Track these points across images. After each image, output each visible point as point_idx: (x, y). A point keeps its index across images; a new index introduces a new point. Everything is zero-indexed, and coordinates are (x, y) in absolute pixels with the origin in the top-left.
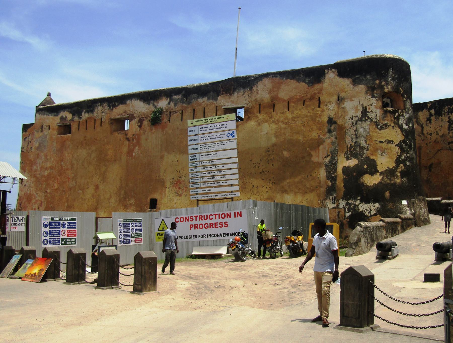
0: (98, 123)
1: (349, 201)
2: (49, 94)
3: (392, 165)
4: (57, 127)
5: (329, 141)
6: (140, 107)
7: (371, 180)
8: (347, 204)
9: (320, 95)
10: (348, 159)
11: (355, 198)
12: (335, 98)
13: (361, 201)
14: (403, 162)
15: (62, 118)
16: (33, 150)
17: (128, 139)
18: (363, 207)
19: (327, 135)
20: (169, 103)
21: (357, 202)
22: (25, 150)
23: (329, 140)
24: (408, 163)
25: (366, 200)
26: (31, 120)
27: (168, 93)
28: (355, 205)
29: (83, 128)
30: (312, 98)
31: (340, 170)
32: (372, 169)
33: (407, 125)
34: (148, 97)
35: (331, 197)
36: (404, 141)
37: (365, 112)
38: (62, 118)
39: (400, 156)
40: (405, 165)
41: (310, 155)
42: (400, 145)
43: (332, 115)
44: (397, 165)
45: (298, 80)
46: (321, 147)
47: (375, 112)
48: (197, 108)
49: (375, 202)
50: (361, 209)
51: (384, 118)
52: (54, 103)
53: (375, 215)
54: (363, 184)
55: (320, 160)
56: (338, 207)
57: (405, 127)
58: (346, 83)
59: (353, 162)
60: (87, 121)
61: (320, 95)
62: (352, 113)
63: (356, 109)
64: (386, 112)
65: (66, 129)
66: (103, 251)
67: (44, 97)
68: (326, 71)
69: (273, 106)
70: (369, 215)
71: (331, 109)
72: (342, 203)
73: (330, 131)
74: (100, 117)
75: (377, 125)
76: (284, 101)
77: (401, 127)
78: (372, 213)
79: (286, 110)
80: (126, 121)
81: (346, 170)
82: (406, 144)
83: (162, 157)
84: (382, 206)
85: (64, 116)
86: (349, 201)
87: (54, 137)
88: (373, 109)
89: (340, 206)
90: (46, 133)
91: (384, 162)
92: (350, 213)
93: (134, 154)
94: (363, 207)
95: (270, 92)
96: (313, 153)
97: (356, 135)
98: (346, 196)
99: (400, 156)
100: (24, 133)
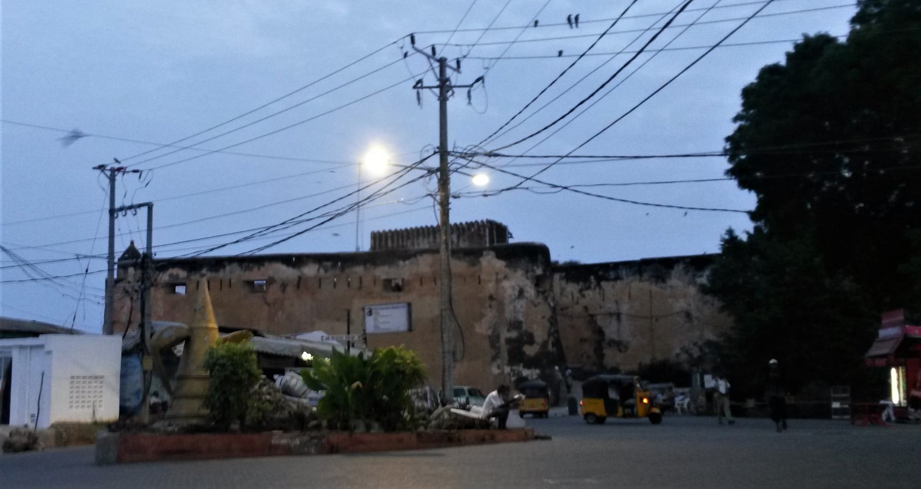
2: (132, 243)
6: (639, 285)
7: (530, 351)
8: (512, 370)
10: (509, 330)
12: (494, 277)
13: (524, 367)
15: (171, 276)
17: (268, 304)
18: (526, 372)
19: (489, 310)
20: (318, 270)
21: (521, 369)
23: (490, 315)
31: (503, 341)
32: (531, 340)
37: (521, 293)
38: (171, 276)
39: (550, 330)
45: (460, 259)
46: (483, 320)
47: (530, 291)
49: (536, 368)
51: (537, 296)
56: (503, 373)
57: (552, 304)
58: (500, 264)
59: (514, 334)
62: (509, 292)
63: (513, 288)
68: (485, 253)
71: (490, 287)
72: (507, 369)
73: (491, 306)
75: (532, 303)
77: (549, 305)
80: (893, 371)
81: (509, 341)
94: (526, 372)
98: (511, 362)
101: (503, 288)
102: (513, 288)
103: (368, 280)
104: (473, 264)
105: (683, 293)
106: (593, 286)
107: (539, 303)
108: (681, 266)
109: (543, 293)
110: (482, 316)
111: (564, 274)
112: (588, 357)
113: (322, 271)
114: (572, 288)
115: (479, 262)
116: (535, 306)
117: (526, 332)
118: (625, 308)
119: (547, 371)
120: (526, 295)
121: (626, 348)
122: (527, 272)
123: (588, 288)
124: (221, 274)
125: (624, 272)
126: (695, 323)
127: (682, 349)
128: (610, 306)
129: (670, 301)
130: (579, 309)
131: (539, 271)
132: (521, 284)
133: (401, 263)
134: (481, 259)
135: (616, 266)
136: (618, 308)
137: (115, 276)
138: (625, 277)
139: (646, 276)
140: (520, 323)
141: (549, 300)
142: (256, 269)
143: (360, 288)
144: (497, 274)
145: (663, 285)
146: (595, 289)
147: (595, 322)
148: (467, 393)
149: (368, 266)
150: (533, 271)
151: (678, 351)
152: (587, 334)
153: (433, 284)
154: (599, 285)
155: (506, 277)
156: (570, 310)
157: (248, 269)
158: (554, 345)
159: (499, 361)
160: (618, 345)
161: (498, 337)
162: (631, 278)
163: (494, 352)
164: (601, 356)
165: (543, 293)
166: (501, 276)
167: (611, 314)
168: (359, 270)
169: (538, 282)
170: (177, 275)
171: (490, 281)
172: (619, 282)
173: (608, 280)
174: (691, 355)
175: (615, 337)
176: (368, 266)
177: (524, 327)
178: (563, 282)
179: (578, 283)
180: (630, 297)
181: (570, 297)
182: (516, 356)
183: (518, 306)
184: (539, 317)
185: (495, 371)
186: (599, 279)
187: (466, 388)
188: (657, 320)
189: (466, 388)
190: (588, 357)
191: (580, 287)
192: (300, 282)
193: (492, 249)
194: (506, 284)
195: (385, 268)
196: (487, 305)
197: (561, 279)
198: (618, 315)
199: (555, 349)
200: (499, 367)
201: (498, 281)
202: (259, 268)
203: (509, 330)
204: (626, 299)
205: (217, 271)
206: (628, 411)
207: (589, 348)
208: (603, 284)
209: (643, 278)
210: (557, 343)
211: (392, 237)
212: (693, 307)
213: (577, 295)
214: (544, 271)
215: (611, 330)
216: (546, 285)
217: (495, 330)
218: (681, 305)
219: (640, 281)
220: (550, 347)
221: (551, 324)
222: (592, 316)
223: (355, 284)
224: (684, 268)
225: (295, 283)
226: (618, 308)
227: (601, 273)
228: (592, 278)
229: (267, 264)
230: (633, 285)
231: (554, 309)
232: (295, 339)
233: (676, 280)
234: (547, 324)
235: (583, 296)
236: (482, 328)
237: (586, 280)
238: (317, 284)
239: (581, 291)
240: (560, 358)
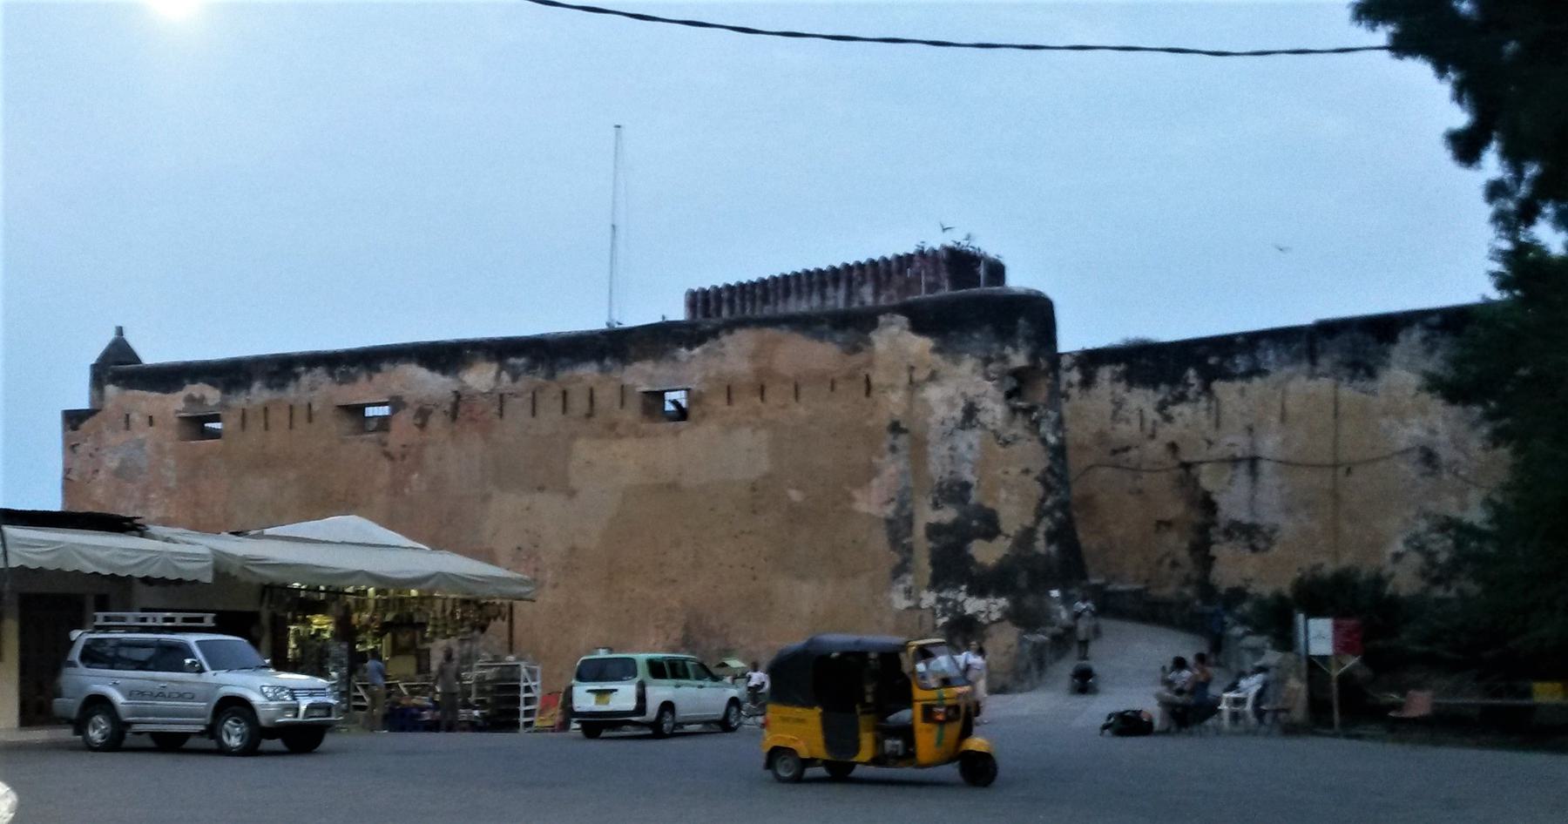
0: (300, 414)
1: (943, 595)
2: (120, 331)
3: (1029, 521)
4: (175, 421)
5: (892, 469)
6: (1304, 386)
7: (986, 553)
8: (939, 600)
9: (868, 371)
10: (936, 506)
11: (956, 587)
13: (970, 593)
14: (1049, 513)
15: (190, 399)
16: (102, 476)
17: (388, 455)
18: (973, 605)
19: (889, 457)
21: (961, 597)
22: (74, 477)
23: (892, 468)
24: (1058, 515)
25: (979, 590)
26: (81, 400)
27: (500, 350)
28: (955, 601)
29: (256, 426)
30: (851, 377)
32: (989, 526)
33: (1054, 433)
34: (444, 356)
35: (901, 587)
36: (1050, 470)
37: (971, 412)
38: (190, 399)
39: (1043, 500)
40: (1052, 517)
41: (851, 499)
42: (1042, 480)
43: (898, 413)
44: (1039, 518)
45: (820, 337)
46: (875, 482)
47: (994, 410)
48: (572, 388)
49: (998, 595)
50: (969, 610)
52: (137, 360)
53: (999, 621)
54: (971, 558)
55: (875, 510)
56: (918, 607)
57: (1052, 439)
58: (920, 345)
59: (948, 515)
60: (266, 410)
61: (868, 371)
62: (941, 411)
63: (951, 403)
64: (1014, 410)
65: (197, 425)
66: (667, 707)
67: (111, 336)
68: (882, 319)
69: (762, 391)
70: (985, 621)
71: (894, 402)
72: (929, 599)
73: (893, 449)
74: (305, 402)
75: (998, 437)
76: (785, 380)
77: (1044, 441)
78: (995, 617)
79: (792, 399)
81: (934, 531)
82: (1054, 475)
83: (486, 498)
84: (1016, 603)
85: (197, 395)
86: (943, 595)
87: (168, 445)
88: (987, 403)
89: (924, 605)
90: (141, 436)
91: (1015, 510)
92: (946, 619)
93: (407, 491)
94: (973, 605)
95: (754, 357)
96: (857, 494)
97: (952, 457)
98: (936, 583)
99: (1043, 500)
100: (70, 432)
101: (925, 401)
102: (951, 403)
103: (606, 396)
104: (855, 350)
105: (1405, 407)
106: (1191, 393)
107: (1016, 437)
108: (1417, 334)
109: (1027, 412)
110: (872, 472)
111: (1121, 368)
112: (1174, 564)
113: (505, 377)
114: (1142, 400)
115: (869, 343)
116: (1006, 443)
117: (980, 507)
118: (1269, 445)
119: (1030, 602)
120: (983, 417)
121: (1270, 541)
122: (987, 361)
123: (1181, 398)
124: (291, 393)
125: (1271, 355)
126: (1446, 476)
127: (1407, 542)
128: (1234, 441)
129: (1384, 422)
130: (1156, 449)
131: (1019, 359)
132: (971, 392)
133: (683, 352)
134: (874, 336)
135: (1252, 341)
136: (1253, 446)
137: (370, 412)
138: (1271, 368)
139: (1325, 363)
140: (967, 486)
141: (1043, 429)
142: (363, 378)
143: (590, 415)
144: (912, 368)
145: (1369, 385)
146: (1197, 400)
147: (1196, 481)
148: (643, 672)
149: (608, 362)
150: (1004, 359)
151: (1399, 546)
152: (1175, 509)
153: (757, 400)
154: (1207, 389)
155: (933, 377)
156: (1133, 453)
157: (348, 379)
158: (1051, 537)
159: (909, 579)
160: (1250, 534)
161: (909, 521)
162: (1288, 370)
163: (897, 558)
164: (1205, 560)
165: (1027, 412)
166: (920, 375)
167: (1235, 461)
168: (588, 372)
169: (1018, 386)
170: (202, 399)
171: (893, 387)
172: (1257, 381)
173: (1228, 376)
174: (1430, 555)
175: (1244, 516)
176: (608, 362)
177: (975, 497)
178: (1120, 388)
179: (1156, 387)
180: (1283, 418)
181: (1136, 424)
182: (951, 565)
183: (963, 447)
184: (1014, 471)
185: (900, 602)
186: (1210, 376)
187: (641, 657)
188: (1349, 471)
189: (641, 657)
190: (1174, 564)
191: (1160, 397)
192: (458, 405)
193: (904, 309)
194: (933, 393)
195: (648, 366)
196: (885, 445)
197: (1116, 379)
198: (1254, 462)
199: (1053, 549)
200: (908, 593)
201: (913, 386)
202: (370, 378)
203: (936, 506)
204: (1274, 419)
205: (282, 386)
206: (892, 744)
207: (1177, 544)
208: (1218, 386)
209: (1319, 370)
210: (1064, 534)
211: (731, 302)
212: (1443, 437)
213: (1152, 415)
214: (1033, 357)
215: (1234, 501)
216: (1041, 393)
217: (902, 505)
218: (1411, 432)
219: (1312, 376)
220: (1041, 545)
221: (1048, 488)
222: (1187, 466)
223: (579, 404)
224: (1425, 340)
225: (448, 407)
226: (1253, 446)
227: (1212, 361)
228: (1191, 373)
229: (385, 367)
230: (1292, 386)
231: (1059, 452)
232: (261, 536)
233: (1402, 374)
234: (1038, 489)
235: (1169, 419)
236: (872, 502)
237: (1176, 379)
238: (495, 410)
239: (1162, 407)
240: (1069, 566)
